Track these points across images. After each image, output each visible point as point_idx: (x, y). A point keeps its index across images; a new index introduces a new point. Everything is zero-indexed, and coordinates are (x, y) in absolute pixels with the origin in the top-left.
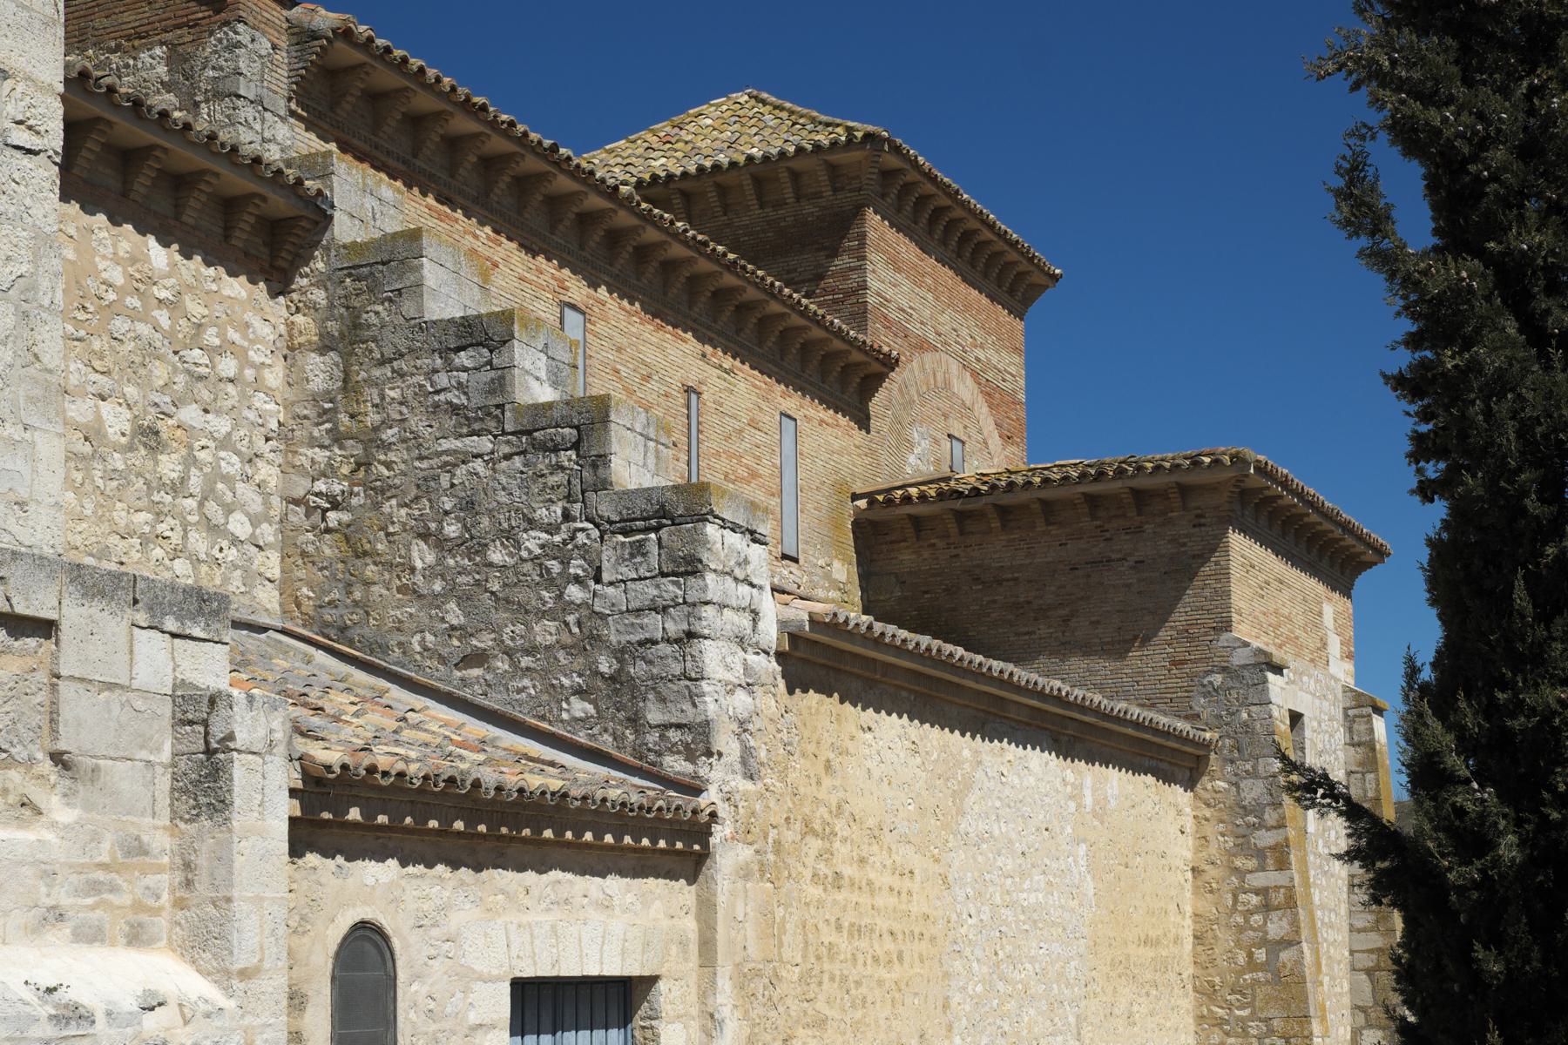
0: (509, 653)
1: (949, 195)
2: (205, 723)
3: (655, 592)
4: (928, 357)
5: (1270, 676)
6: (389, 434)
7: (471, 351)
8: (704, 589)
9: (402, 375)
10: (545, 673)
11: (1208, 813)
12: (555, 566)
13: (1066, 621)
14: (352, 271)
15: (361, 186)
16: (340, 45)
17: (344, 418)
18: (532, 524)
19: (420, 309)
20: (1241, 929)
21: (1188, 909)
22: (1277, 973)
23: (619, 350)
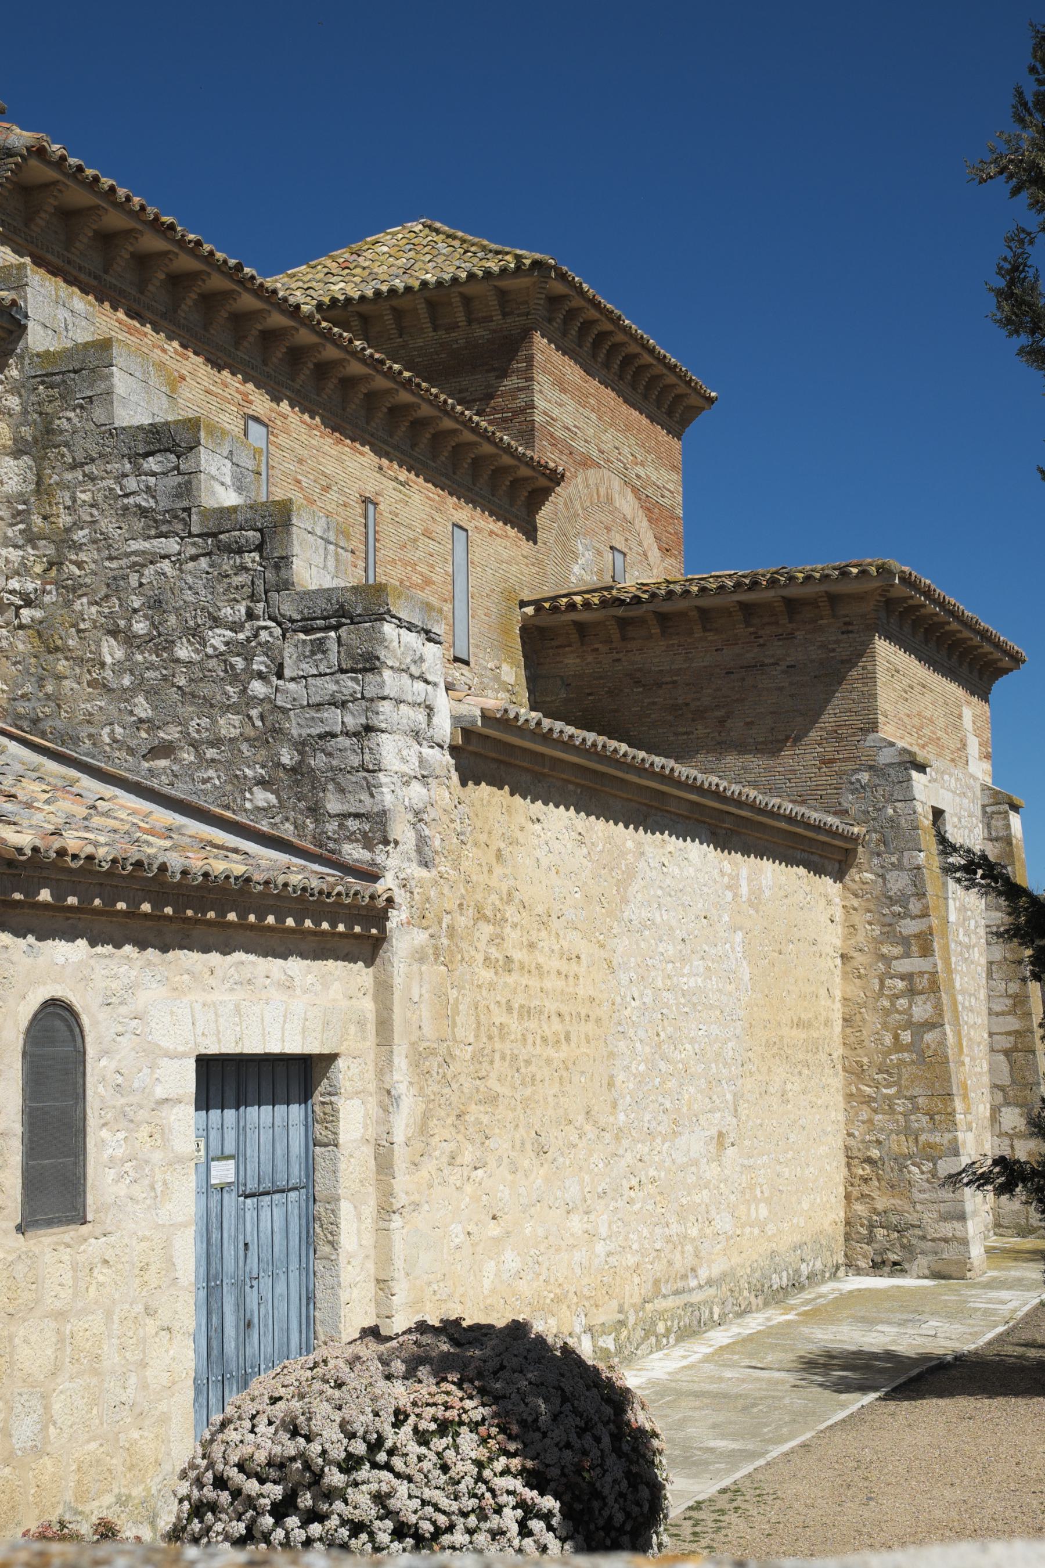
0: (194, 745)
3: (335, 688)
4: (591, 473)
5: (914, 774)
6: (80, 535)
7: (159, 457)
9: (93, 479)
11: (856, 903)
12: (239, 663)
13: (722, 722)
14: (45, 379)
15: (54, 297)
16: (33, 162)
17: (37, 520)
18: (217, 622)
19: (111, 415)
20: (887, 1012)
21: (838, 994)
22: (921, 1053)
23: (301, 461)
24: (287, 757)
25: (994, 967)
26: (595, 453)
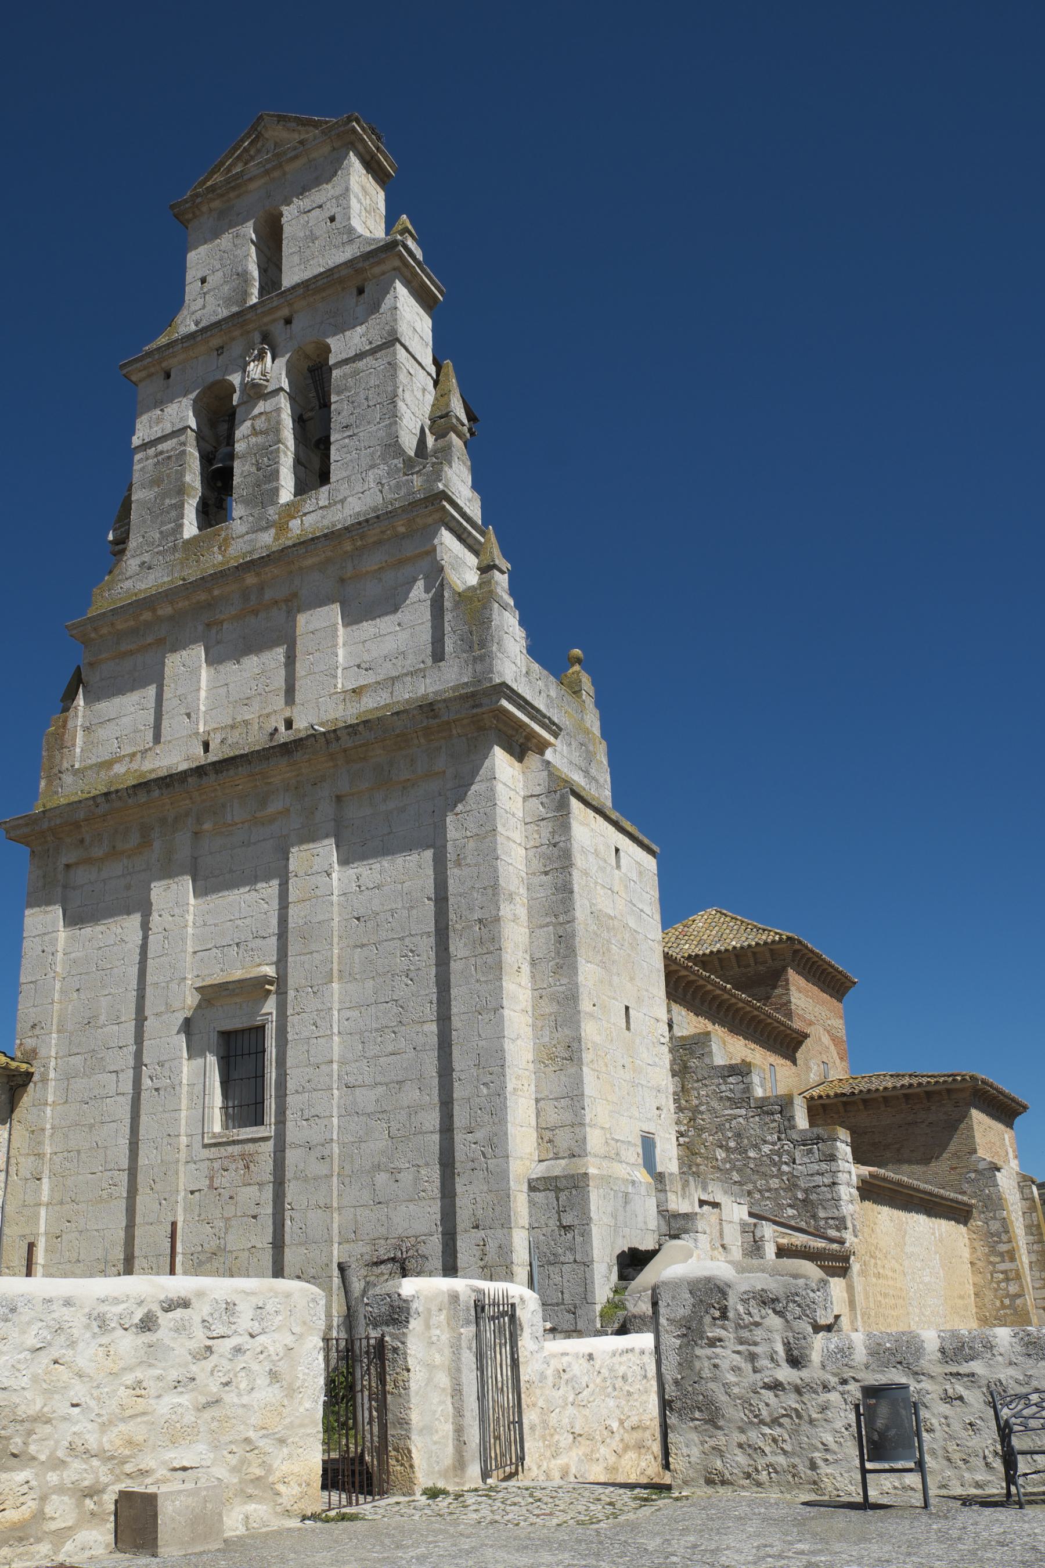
0: (760, 1191)
1: (817, 957)
2: (753, 1232)
5: (997, 1173)
6: (703, 1108)
7: (734, 1077)
8: (838, 1166)
9: (706, 1086)
10: (775, 1199)
11: (975, 1236)
12: (776, 1158)
13: (898, 1150)
14: (682, 1047)
17: (683, 1102)
18: (765, 1142)
19: (712, 1061)
20: (996, 1290)
21: (971, 1281)
22: (1015, 1310)
24: (800, 1195)
25: (1033, 1265)
26: (813, 1018)
